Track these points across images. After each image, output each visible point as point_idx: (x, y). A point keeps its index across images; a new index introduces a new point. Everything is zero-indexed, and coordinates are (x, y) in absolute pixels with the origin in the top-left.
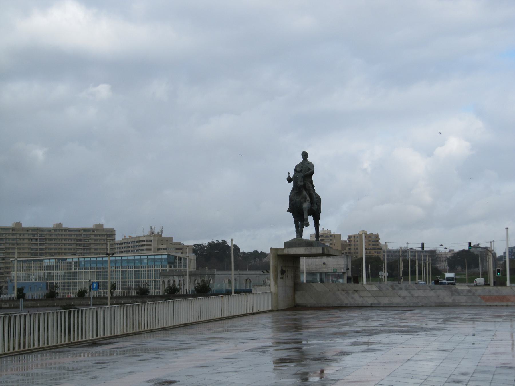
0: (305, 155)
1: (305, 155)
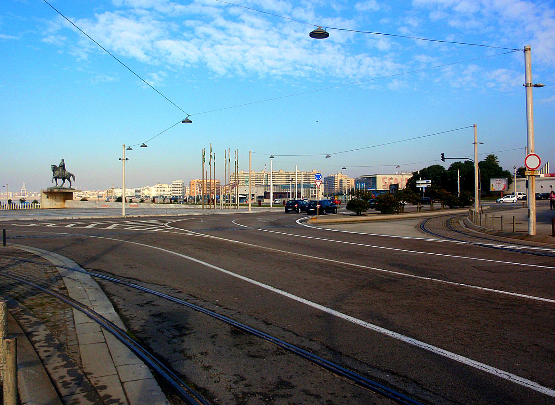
0: (63, 160)
1: (63, 160)
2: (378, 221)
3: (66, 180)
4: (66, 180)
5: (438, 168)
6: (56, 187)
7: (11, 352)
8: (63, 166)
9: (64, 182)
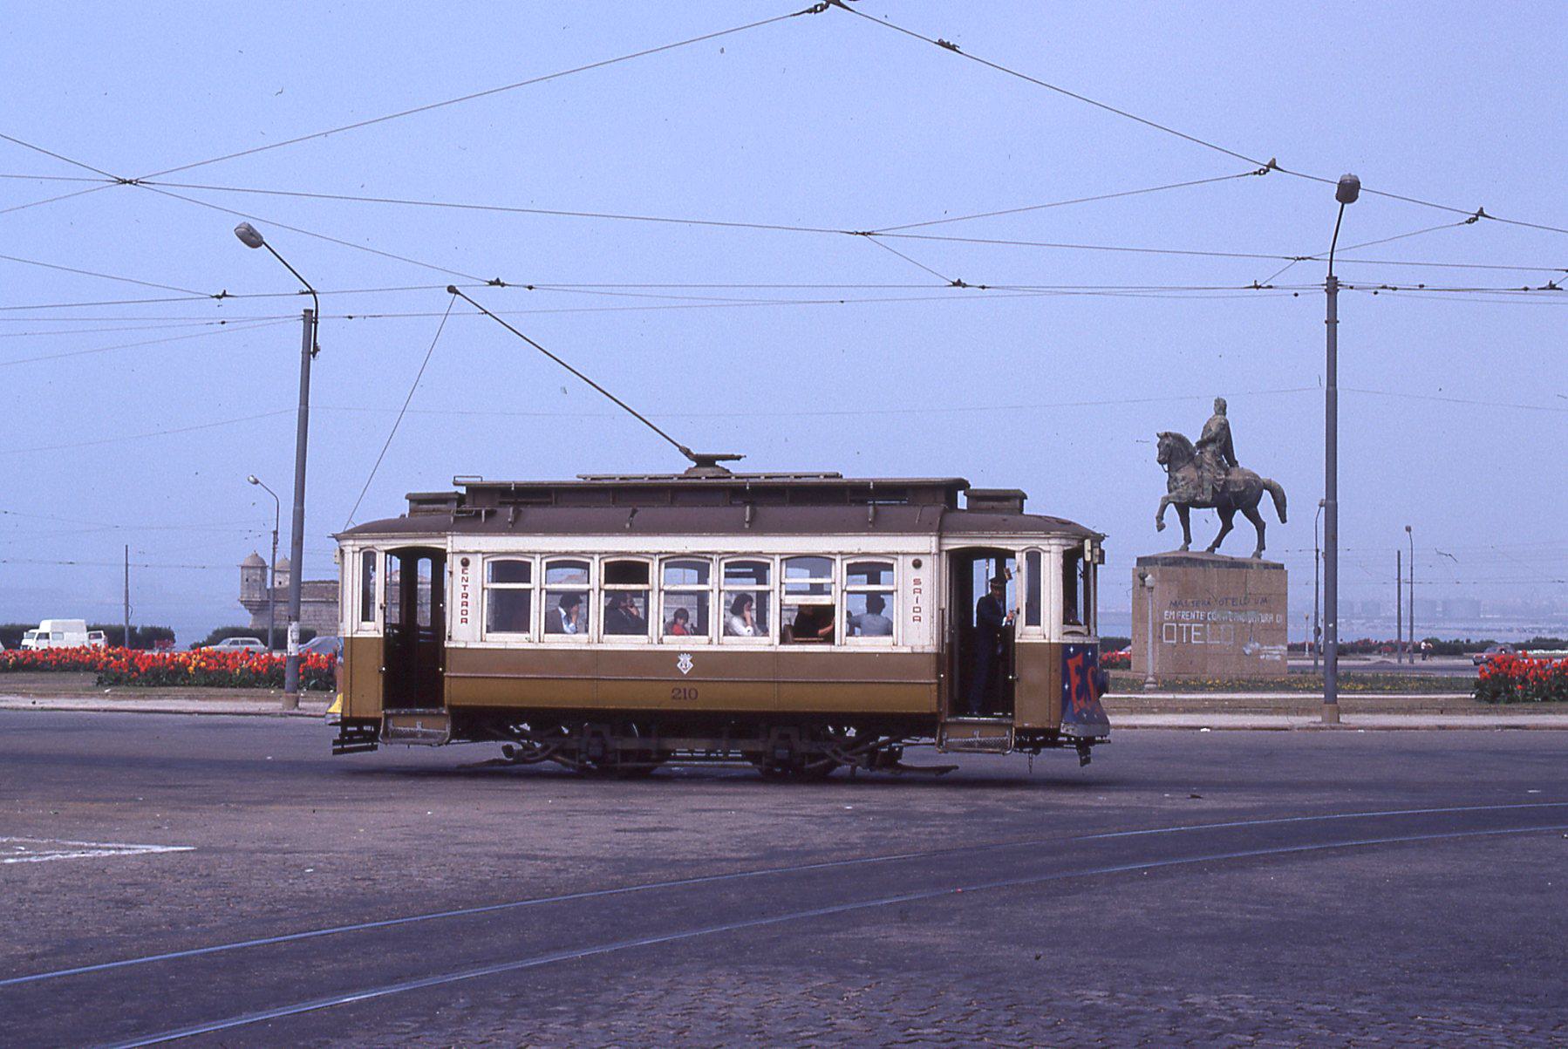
0: (1221, 407)
1: (1221, 407)
2: (985, 504)
3: (1239, 512)
4: (1239, 517)
5: (1437, 640)
6: (1184, 555)
7: (734, 984)
8: (1220, 440)
9: (1227, 526)
